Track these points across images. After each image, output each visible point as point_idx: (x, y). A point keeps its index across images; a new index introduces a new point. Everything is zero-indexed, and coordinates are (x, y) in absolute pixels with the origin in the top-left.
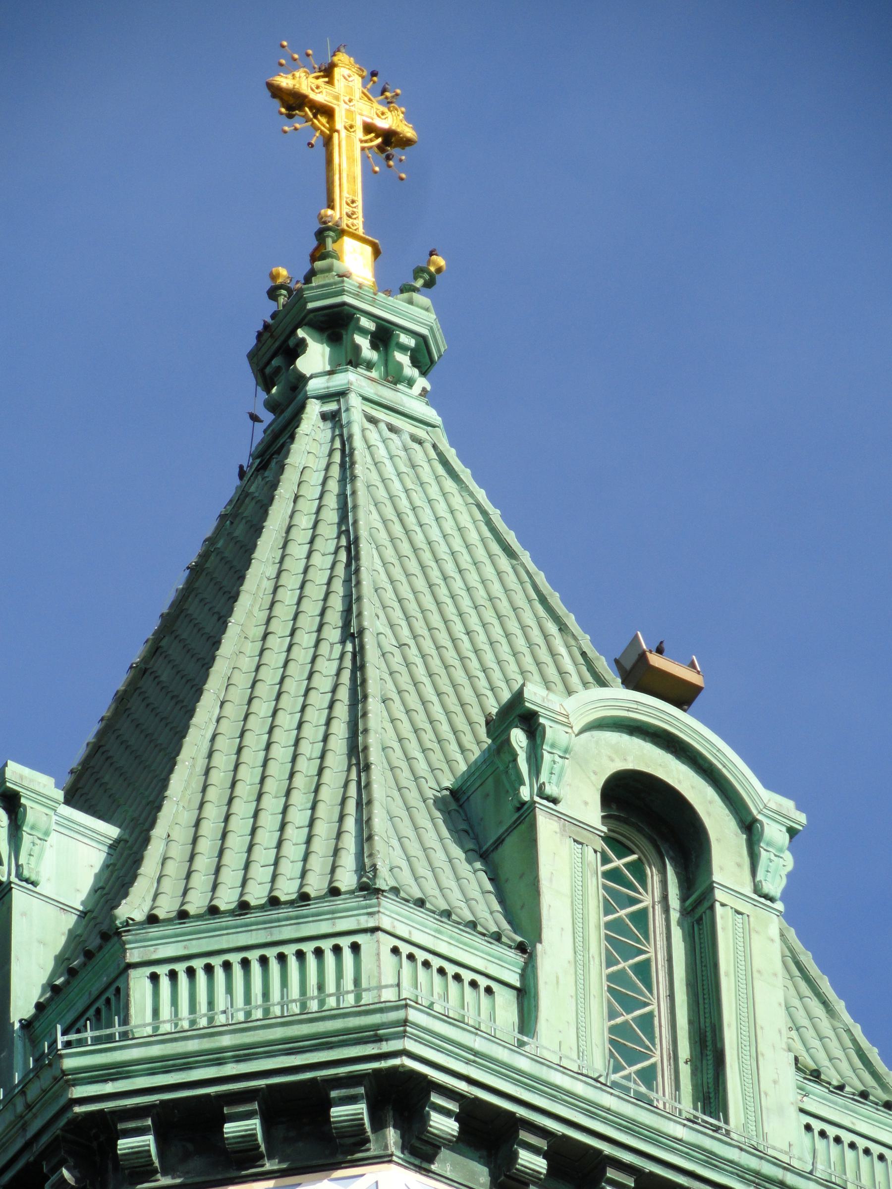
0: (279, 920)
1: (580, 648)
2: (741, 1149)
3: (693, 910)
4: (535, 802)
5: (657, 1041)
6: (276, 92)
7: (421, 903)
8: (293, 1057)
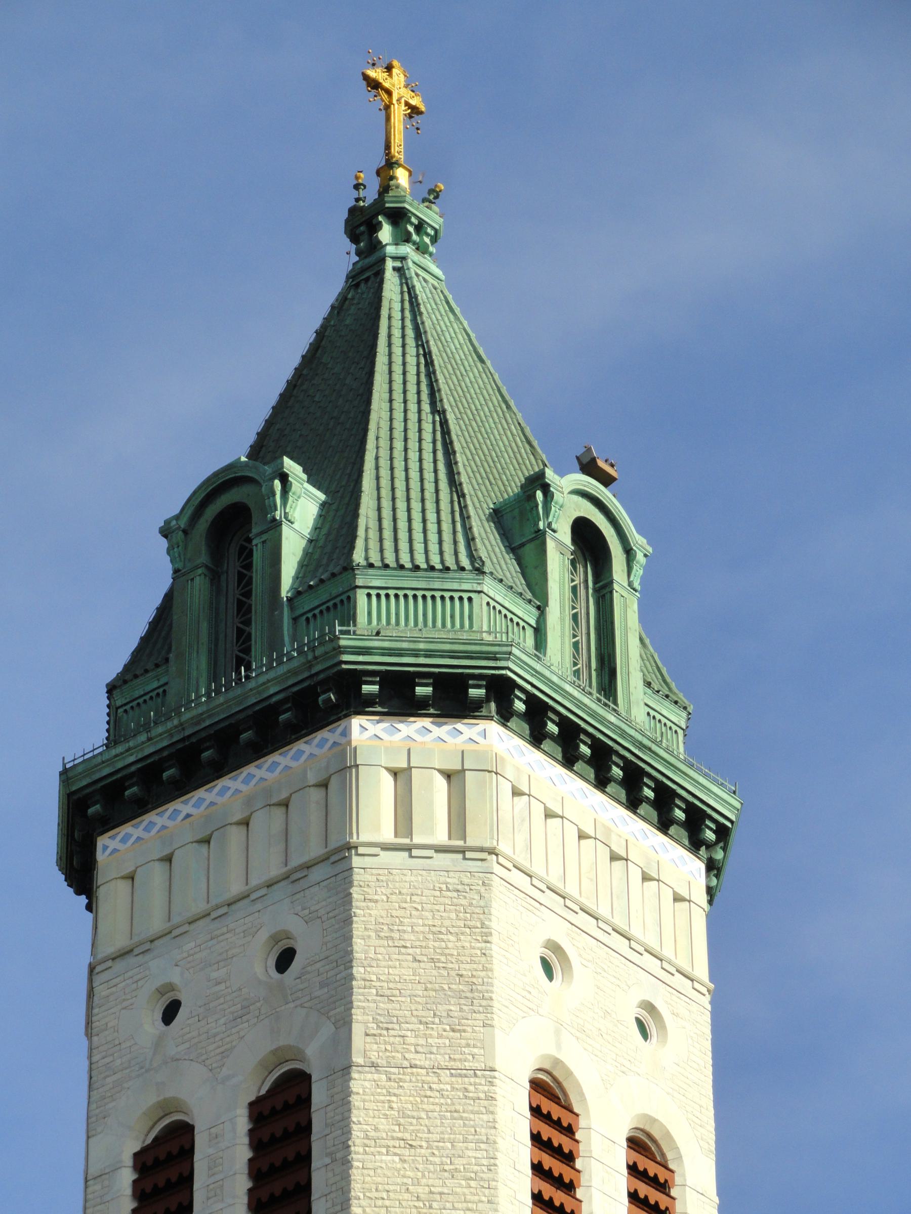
0: (433, 578)
1: (517, 420)
2: (636, 730)
3: (599, 590)
4: (546, 531)
5: (581, 656)
6: (366, 77)
7: (501, 581)
8: (453, 660)
